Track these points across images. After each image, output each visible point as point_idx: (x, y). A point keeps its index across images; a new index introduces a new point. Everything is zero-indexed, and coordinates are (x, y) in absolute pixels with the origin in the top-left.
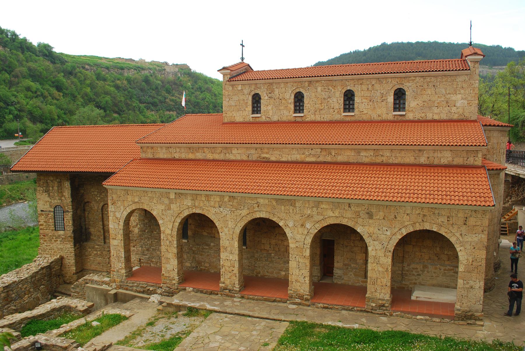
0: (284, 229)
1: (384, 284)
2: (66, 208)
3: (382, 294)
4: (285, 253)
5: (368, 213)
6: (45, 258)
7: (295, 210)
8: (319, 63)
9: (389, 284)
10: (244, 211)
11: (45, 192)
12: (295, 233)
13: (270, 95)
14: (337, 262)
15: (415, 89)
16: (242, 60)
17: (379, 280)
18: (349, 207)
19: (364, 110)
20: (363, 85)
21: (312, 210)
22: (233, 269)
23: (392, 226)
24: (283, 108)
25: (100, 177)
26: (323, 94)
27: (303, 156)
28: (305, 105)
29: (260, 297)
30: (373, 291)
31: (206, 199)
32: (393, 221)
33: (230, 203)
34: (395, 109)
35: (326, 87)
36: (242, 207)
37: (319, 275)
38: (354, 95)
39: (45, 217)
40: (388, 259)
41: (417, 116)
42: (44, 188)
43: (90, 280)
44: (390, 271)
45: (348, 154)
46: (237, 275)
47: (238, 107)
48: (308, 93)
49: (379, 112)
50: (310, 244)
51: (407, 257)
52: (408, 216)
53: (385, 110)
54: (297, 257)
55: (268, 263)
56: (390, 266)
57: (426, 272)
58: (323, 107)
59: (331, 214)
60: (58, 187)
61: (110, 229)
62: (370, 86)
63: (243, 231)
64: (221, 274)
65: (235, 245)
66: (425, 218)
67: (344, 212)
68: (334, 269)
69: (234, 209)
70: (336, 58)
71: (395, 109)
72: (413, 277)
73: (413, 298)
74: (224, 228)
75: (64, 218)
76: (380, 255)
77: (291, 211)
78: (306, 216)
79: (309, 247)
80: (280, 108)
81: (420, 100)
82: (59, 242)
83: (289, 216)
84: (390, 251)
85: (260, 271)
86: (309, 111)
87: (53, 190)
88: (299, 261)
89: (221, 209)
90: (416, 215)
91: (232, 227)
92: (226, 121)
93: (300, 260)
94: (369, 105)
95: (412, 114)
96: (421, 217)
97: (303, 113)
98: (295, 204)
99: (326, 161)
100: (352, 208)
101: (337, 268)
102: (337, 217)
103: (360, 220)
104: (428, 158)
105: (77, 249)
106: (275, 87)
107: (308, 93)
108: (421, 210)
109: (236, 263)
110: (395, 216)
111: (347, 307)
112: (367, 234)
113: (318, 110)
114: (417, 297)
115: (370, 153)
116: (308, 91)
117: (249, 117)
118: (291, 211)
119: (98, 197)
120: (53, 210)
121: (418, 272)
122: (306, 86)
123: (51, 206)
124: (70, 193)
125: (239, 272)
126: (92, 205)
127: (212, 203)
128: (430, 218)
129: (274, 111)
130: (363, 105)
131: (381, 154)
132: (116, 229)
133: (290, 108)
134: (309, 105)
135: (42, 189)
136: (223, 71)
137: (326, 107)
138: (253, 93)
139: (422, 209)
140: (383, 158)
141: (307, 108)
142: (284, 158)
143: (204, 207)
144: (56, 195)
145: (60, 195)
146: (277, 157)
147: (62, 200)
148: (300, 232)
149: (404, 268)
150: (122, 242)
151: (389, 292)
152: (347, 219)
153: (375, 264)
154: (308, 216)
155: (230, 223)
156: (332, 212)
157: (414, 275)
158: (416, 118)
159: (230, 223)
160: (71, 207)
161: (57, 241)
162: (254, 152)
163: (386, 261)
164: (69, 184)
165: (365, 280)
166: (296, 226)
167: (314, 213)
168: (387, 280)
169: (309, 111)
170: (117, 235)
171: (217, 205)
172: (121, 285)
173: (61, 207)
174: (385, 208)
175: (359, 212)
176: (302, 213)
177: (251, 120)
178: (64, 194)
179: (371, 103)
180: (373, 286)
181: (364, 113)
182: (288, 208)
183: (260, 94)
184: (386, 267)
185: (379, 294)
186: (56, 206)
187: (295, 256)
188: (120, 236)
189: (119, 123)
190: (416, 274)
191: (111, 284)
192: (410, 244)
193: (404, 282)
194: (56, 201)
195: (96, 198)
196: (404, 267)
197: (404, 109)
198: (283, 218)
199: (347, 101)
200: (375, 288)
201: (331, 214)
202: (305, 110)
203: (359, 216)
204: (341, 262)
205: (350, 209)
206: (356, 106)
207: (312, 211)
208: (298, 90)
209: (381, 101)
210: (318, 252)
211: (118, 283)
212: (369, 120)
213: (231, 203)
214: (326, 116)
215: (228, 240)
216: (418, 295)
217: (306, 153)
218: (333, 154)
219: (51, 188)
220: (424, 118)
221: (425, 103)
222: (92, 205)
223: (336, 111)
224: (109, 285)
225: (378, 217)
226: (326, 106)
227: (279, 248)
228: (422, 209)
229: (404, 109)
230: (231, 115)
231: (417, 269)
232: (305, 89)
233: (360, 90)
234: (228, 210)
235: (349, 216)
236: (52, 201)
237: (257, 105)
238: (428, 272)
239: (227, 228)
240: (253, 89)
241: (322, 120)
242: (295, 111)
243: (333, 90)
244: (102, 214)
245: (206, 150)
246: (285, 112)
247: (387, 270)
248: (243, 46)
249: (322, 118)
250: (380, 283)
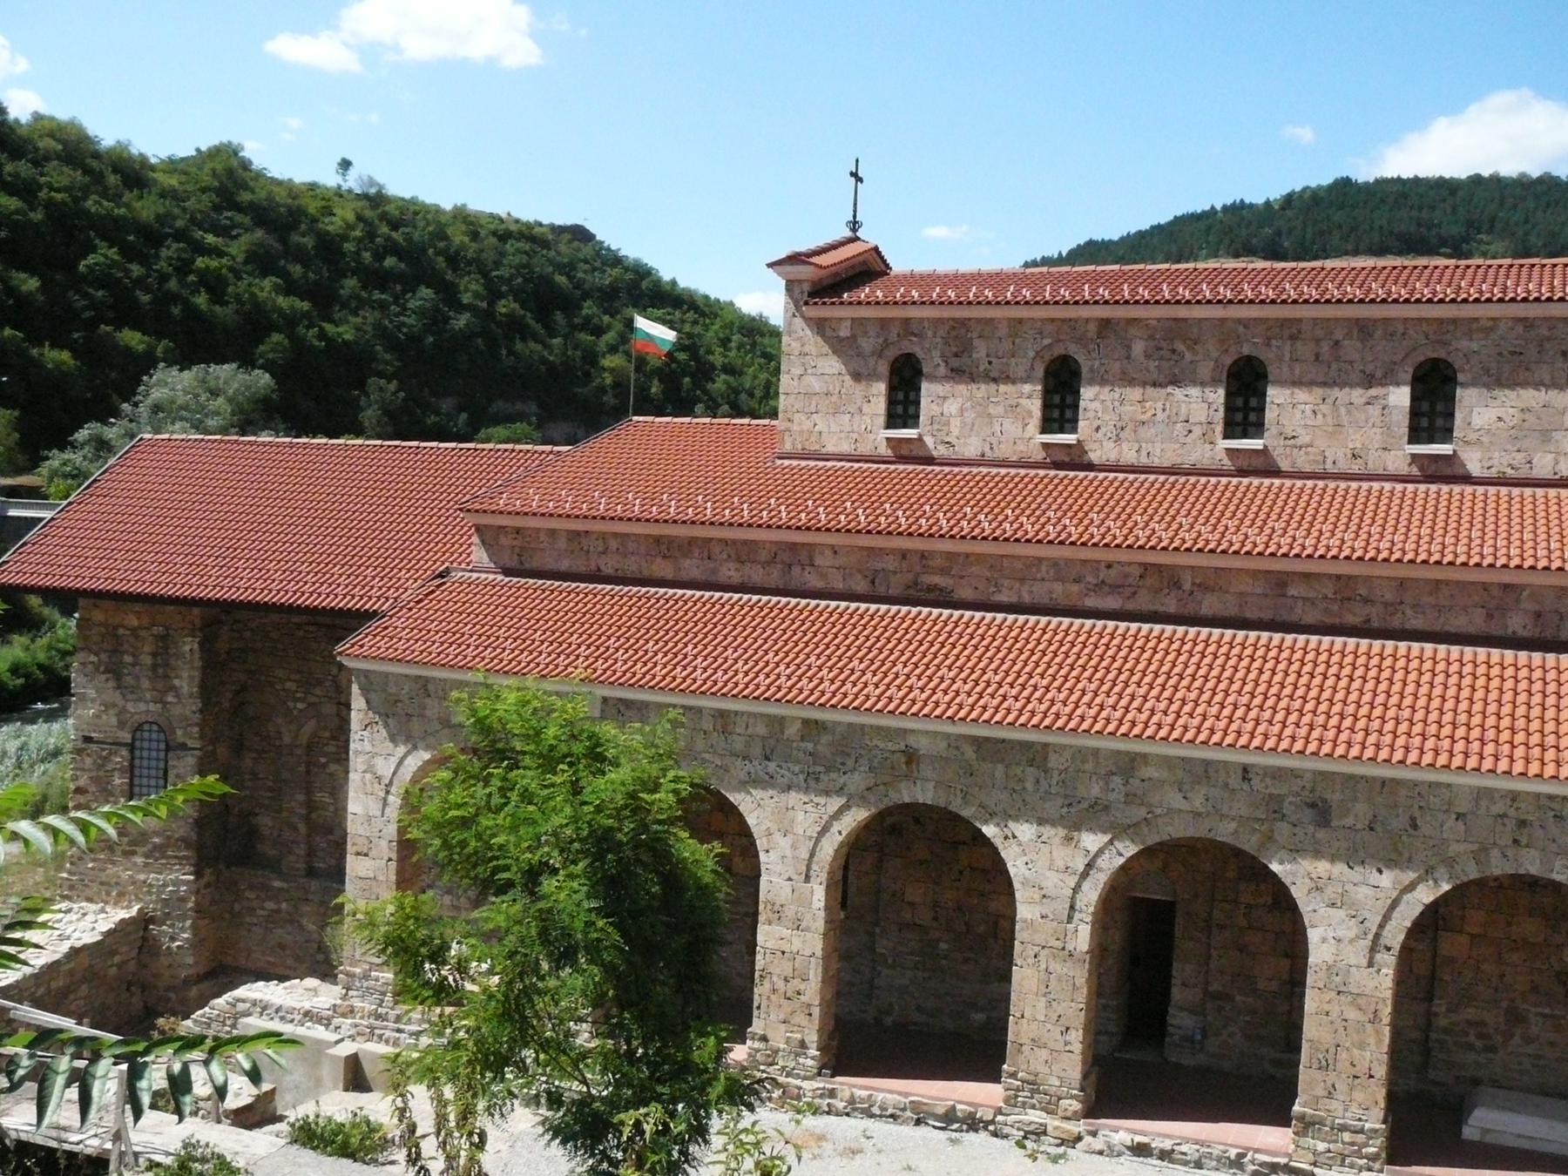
0: (1000, 848)
1: (1362, 1068)
2: (179, 732)
3: (1354, 1108)
4: (991, 940)
5: (1313, 805)
6: (84, 915)
7: (1044, 783)
8: (1090, 243)
9: (1381, 1071)
10: (856, 776)
11: (107, 671)
12: (1039, 864)
13: (955, 363)
14: (1183, 984)
15: (1493, 365)
16: (854, 230)
17: (1343, 1055)
18: (1244, 778)
19: (1300, 431)
20: (1299, 344)
21: (1107, 783)
22: (802, 987)
23: (1400, 854)
24: (1000, 409)
25: (311, 628)
26: (1152, 368)
27: (1075, 588)
28: (1082, 404)
29: (898, 1098)
30: (1320, 1091)
31: (719, 727)
32: (1404, 838)
33: (803, 745)
34: (1415, 436)
35: (1164, 344)
36: (850, 763)
37: (1113, 1028)
38: (1266, 377)
39: (95, 762)
40: (1381, 978)
41: (1495, 462)
42: (104, 656)
43: (254, 1003)
44: (1386, 1020)
45: (1242, 588)
46: (816, 1011)
47: (834, 399)
48: (1097, 363)
49: (1356, 440)
50: (1092, 909)
51: (1447, 978)
52: (1460, 823)
53: (1378, 437)
54: (1044, 953)
55: (926, 975)
56: (1389, 1002)
57: (1517, 1039)
58: (1149, 414)
59: (1176, 801)
60: (154, 655)
61: (350, 817)
62: (1325, 347)
63: (845, 850)
64: (756, 1004)
65: (815, 898)
66: (1526, 831)
67: (1226, 795)
68: (1171, 1011)
69: (819, 769)
70: (1157, 229)
71: (1415, 436)
72: (1471, 1057)
73: (1469, 1132)
74: (778, 836)
75: (166, 772)
76: (1353, 961)
77: (1029, 785)
78: (1085, 805)
79: (1089, 919)
80: (991, 411)
81: (1508, 404)
82: (139, 860)
83: (1020, 804)
84: (1389, 949)
85: (891, 1005)
86: (1098, 429)
87: (134, 665)
88: (1051, 969)
89: (772, 766)
90: (1490, 821)
91: (808, 834)
92: (788, 447)
93: (1056, 967)
94: (1319, 416)
95: (1478, 455)
96: (1508, 828)
97: (1074, 430)
98: (1046, 759)
99: (1162, 609)
100: (1256, 781)
101: (1182, 1009)
102: (1199, 814)
103: (1283, 829)
104: (1538, 615)
105: (208, 885)
106: (975, 335)
107: (1097, 363)
108: (1509, 803)
109: (812, 965)
110: (1413, 819)
111: (1222, 1147)
112: (1307, 880)
113: (1131, 426)
114: (1485, 1131)
115: (1324, 590)
116: (1094, 355)
117: (872, 437)
118: (1029, 785)
119: (296, 700)
120: (130, 736)
121: (1488, 1037)
122: (1090, 335)
123: (121, 725)
124: (197, 680)
125: (822, 999)
126: (271, 728)
127: (739, 743)
128: (1541, 831)
129: (969, 421)
130: (1298, 415)
131: (1363, 591)
132: (369, 819)
133: (1030, 413)
134: (1096, 405)
135: (93, 658)
136: (789, 268)
137: (1161, 416)
138: (892, 353)
139: (1514, 800)
140: (1368, 609)
141: (1091, 414)
142: (1005, 591)
143: (707, 756)
144: (146, 684)
145: (160, 686)
146: (980, 588)
147: (165, 704)
148: (1060, 864)
149: (1433, 1019)
150: (393, 865)
151: (1382, 1104)
152: (1233, 825)
153: (1333, 994)
154: (1091, 807)
155: (800, 816)
156: (1179, 796)
157: (1471, 1047)
158: (1493, 470)
159: (800, 816)
160: (196, 729)
161: (134, 853)
162: (896, 564)
163: (1372, 984)
164: (196, 646)
165: (1286, 1056)
166: (1043, 839)
167: (1112, 796)
168: (1374, 1053)
169: (1098, 429)
170: (375, 840)
171: (757, 751)
172: (372, 1028)
173: (161, 730)
174: (1378, 789)
175: (1279, 799)
176: (1068, 792)
177: (884, 450)
178: (176, 682)
179: (1325, 408)
180: (1319, 1075)
181: (1299, 442)
182: (1019, 772)
183: (920, 354)
184: (1372, 1008)
185: (1341, 1108)
186: (141, 725)
187: (1037, 949)
188: (384, 843)
189: (127, 440)
190: (1479, 1044)
191: (337, 1021)
192: (1461, 932)
193: (1432, 1075)
194: (142, 707)
195: (290, 704)
196: (1436, 1015)
197: (1446, 434)
198: (997, 810)
199: (1057, 392)
200: (1329, 1083)
201: (1176, 801)
202: (1081, 424)
203: (1278, 814)
204: (1195, 986)
205: (1245, 786)
206: (1270, 415)
207: (1107, 789)
208: (1059, 350)
209: (1363, 400)
210: (1117, 938)
211: (362, 1018)
212: (1318, 469)
213: (810, 746)
214: (1158, 446)
215: (790, 879)
216: (1483, 1122)
217: (1090, 579)
218: (1187, 586)
219: (128, 659)
220: (1523, 473)
221: (1527, 416)
222: (271, 728)
223: (1197, 431)
224: (327, 1026)
225: (1349, 821)
226: (1159, 412)
227: (966, 924)
228: (1514, 800)
229: (1446, 434)
230: (807, 425)
231: (1483, 1024)
232: (1085, 347)
233: (1287, 357)
234: (797, 769)
235: (1245, 812)
236: (130, 707)
237: (906, 396)
238: (1528, 1040)
239: (790, 836)
240: (893, 337)
241: (1144, 460)
242: (1047, 426)
243: (1188, 356)
244: (308, 764)
245: (717, 550)
246: (1007, 424)
247: (1375, 1018)
248: (859, 179)
249: (1144, 453)
250: (1347, 1064)
